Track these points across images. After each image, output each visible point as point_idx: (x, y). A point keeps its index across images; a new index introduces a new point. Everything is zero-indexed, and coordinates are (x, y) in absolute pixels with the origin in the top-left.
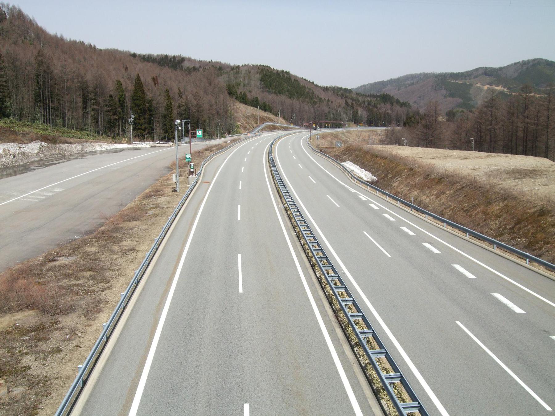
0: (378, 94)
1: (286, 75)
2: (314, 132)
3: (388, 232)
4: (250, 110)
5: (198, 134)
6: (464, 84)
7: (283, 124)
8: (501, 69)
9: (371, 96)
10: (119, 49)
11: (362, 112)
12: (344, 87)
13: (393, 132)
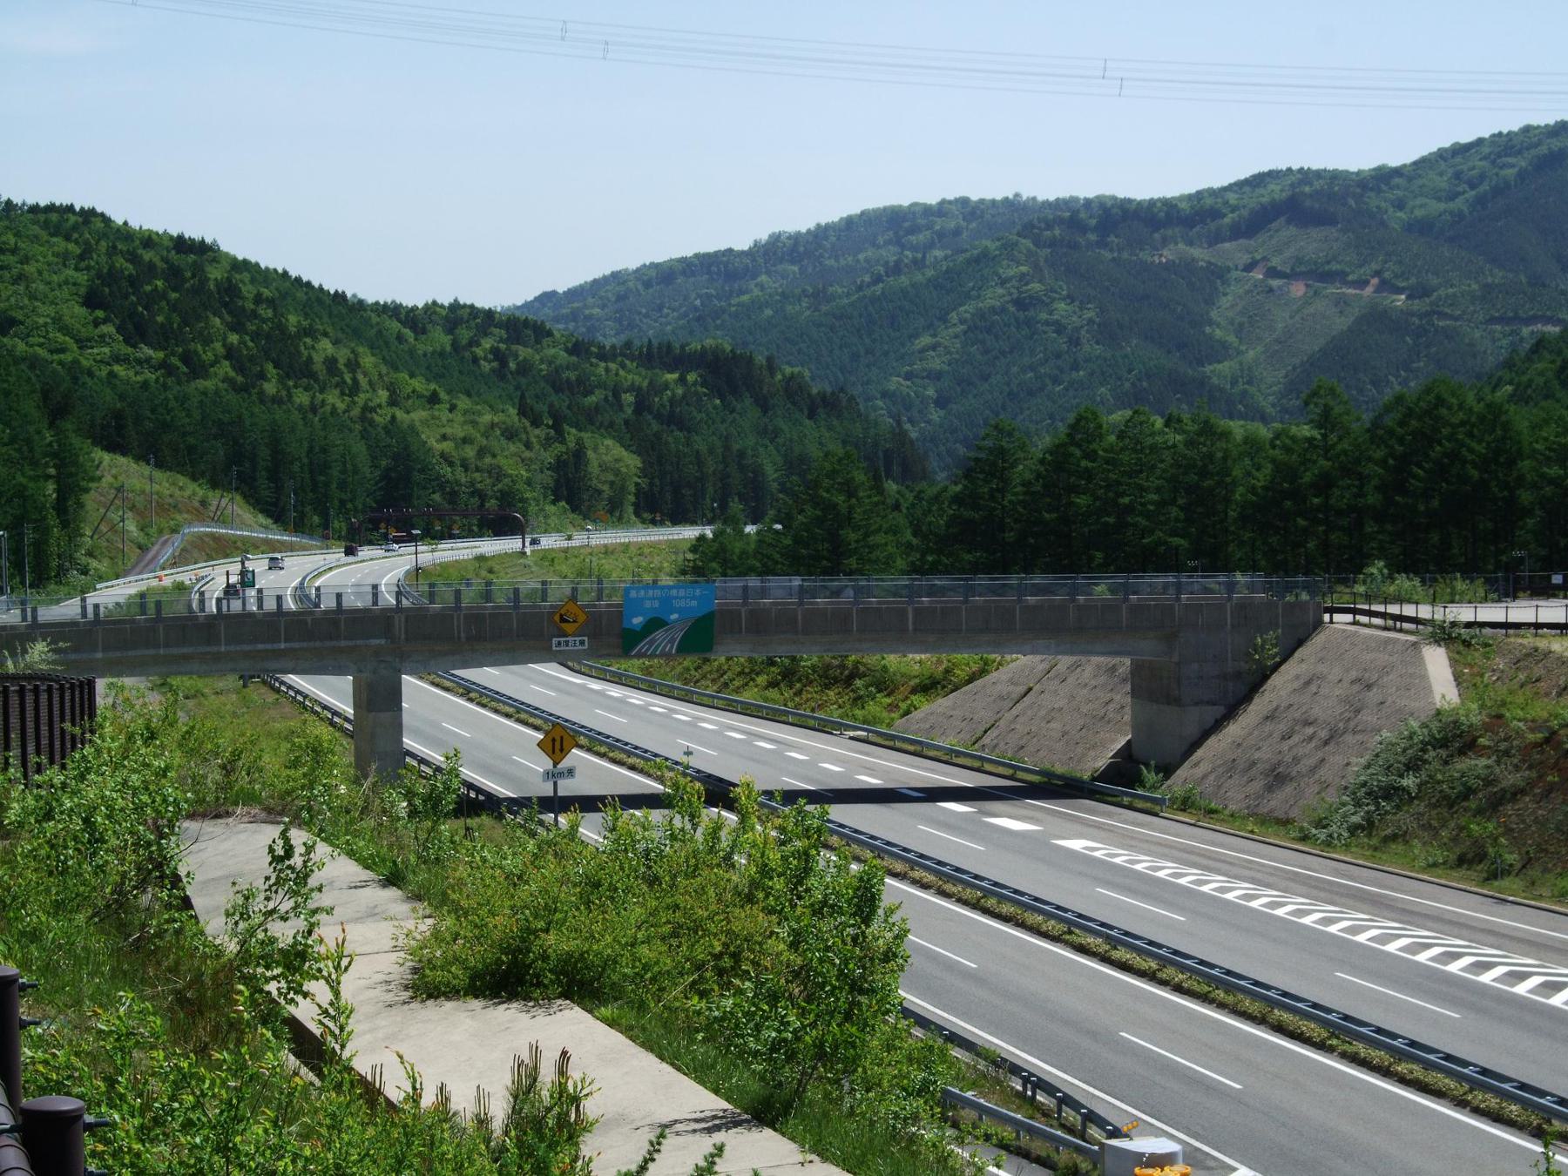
6: (1185, 268)
7: (250, 528)
8: (1383, 177)
11: (611, 457)
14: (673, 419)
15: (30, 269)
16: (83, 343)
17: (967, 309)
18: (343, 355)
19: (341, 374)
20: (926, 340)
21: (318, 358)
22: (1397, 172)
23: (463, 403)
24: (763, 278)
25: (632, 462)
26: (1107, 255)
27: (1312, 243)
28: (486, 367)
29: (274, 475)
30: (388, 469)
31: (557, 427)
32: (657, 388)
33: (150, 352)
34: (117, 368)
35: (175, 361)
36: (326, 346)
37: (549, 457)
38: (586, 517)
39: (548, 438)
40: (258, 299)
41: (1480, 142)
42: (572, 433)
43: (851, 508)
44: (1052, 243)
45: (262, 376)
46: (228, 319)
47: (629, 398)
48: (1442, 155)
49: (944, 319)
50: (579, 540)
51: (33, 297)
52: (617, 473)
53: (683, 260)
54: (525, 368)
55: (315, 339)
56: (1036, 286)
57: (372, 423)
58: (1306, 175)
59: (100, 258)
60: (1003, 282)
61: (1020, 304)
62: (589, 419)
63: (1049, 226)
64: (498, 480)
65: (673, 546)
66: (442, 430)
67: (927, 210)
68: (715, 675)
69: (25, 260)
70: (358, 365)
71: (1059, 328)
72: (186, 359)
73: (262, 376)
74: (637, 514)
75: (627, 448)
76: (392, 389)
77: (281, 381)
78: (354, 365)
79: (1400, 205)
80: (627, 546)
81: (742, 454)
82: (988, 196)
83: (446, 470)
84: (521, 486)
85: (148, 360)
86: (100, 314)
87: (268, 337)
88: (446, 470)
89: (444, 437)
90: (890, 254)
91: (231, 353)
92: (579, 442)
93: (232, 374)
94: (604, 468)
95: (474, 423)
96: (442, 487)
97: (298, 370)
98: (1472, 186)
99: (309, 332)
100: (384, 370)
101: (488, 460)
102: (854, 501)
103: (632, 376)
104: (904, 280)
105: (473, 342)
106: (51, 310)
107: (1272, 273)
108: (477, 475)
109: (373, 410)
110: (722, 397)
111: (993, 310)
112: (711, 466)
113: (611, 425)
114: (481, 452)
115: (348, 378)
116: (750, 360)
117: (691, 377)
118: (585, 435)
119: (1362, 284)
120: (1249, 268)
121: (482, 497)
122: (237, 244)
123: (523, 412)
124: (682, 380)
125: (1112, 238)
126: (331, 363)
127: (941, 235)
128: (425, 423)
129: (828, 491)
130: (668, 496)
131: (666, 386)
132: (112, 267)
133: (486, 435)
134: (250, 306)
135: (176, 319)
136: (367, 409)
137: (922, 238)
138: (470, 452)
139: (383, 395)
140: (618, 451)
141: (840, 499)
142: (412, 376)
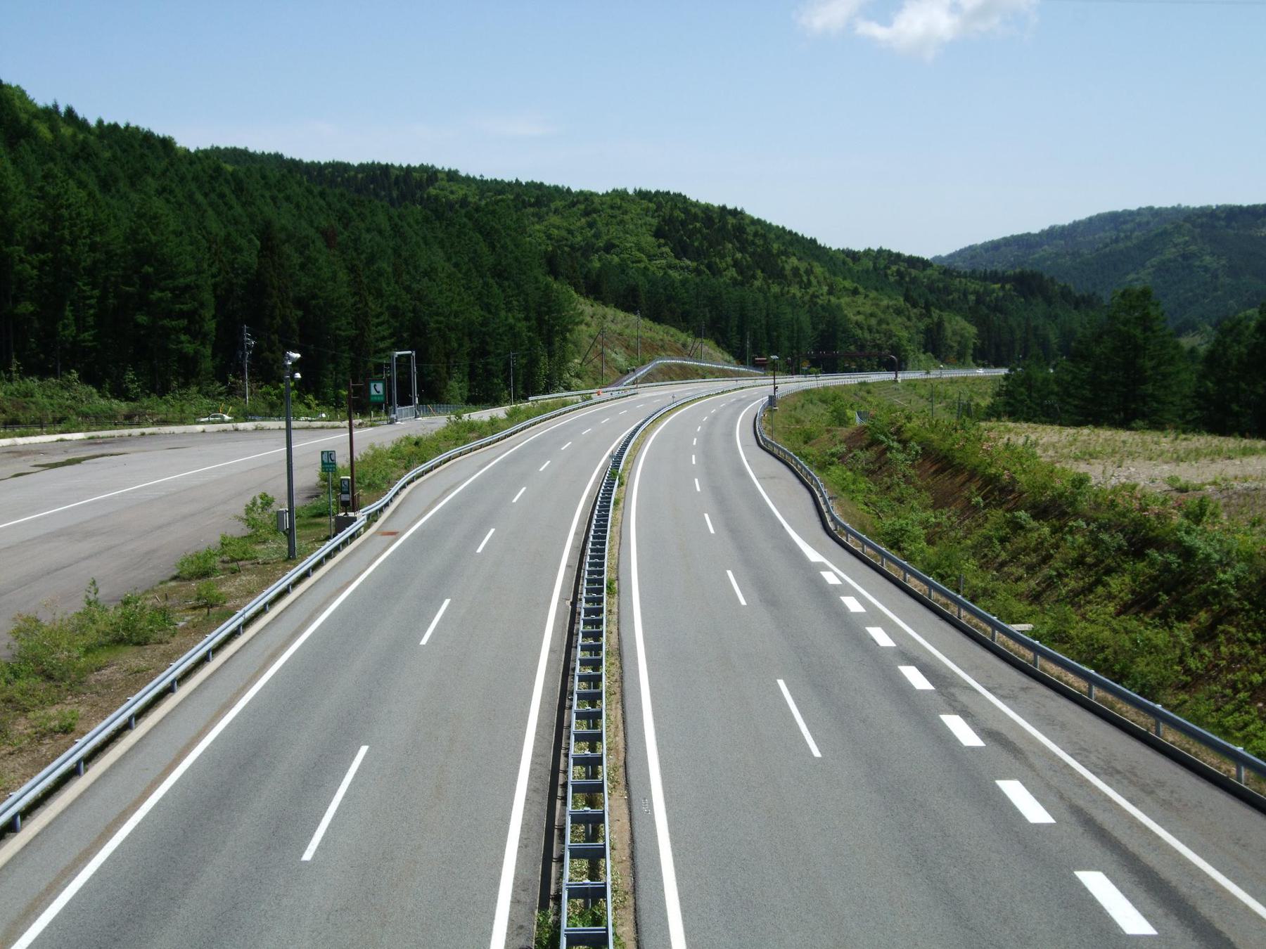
0: (1011, 272)
1: (67, 131)
2: (791, 384)
3: (839, 669)
5: (373, 392)
7: (713, 360)
9: (994, 277)
10: (251, 150)
11: (960, 327)
12: (907, 251)
13: (1027, 382)
14: (997, 308)
15: (627, 217)
16: (651, 258)
17: (1155, 260)
18: (803, 266)
19: (801, 276)
21: (788, 267)
23: (873, 294)
24: (1046, 247)
25: (972, 330)
26: (1231, 232)
28: (892, 279)
29: (741, 331)
30: (823, 331)
31: (927, 307)
32: (988, 293)
33: (689, 262)
34: (670, 272)
35: (702, 267)
36: (794, 261)
37: (922, 326)
38: (943, 362)
39: (921, 315)
40: (756, 234)
42: (936, 313)
43: (1147, 339)
44: (1202, 226)
46: (738, 245)
47: (972, 298)
49: (1143, 266)
50: (934, 374)
52: (962, 336)
53: (1005, 239)
54: (914, 280)
55: (788, 257)
56: (1193, 248)
57: (815, 304)
59: (666, 211)
60: (1175, 246)
61: (1185, 257)
62: (949, 306)
63: (1199, 217)
64: (890, 338)
66: (856, 310)
68: (1034, 558)
69: (625, 213)
70: (812, 272)
71: (1206, 269)
72: (709, 267)
73: (754, 277)
74: (974, 360)
75: (969, 322)
77: (764, 279)
78: (809, 272)
80: (966, 378)
81: (1036, 328)
82: (1164, 205)
84: (905, 343)
85: (687, 267)
86: (662, 241)
87: (760, 256)
89: (859, 313)
90: (1114, 234)
91: (736, 264)
92: (940, 317)
93: (735, 275)
94: (954, 333)
95: (877, 305)
96: (855, 342)
99: (785, 253)
100: (827, 275)
101: (884, 326)
103: (974, 286)
104: (1121, 245)
105: (887, 267)
108: (877, 336)
109: (817, 297)
110: (1025, 297)
111: (1170, 260)
112: (1018, 334)
113: (961, 309)
114: (880, 322)
115: (805, 279)
116: (1041, 276)
117: (1008, 286)
118: (945, 315)
121: (880, 348)
123: (907, 299)
124: (1003, 288)
125: (1234, 224)
126: (796, 271)
127: (1139, 225)
128: (848, 305)
130: (993, 351)
131: (994, 291)
132: (671, 215)
133: (884, 312)
134: (750, 238)
135: (706, 244)
137: (1129, 226)
138: (873, 321)
139: (825, 289)
141: (1138, 332)
142: (845, 279)
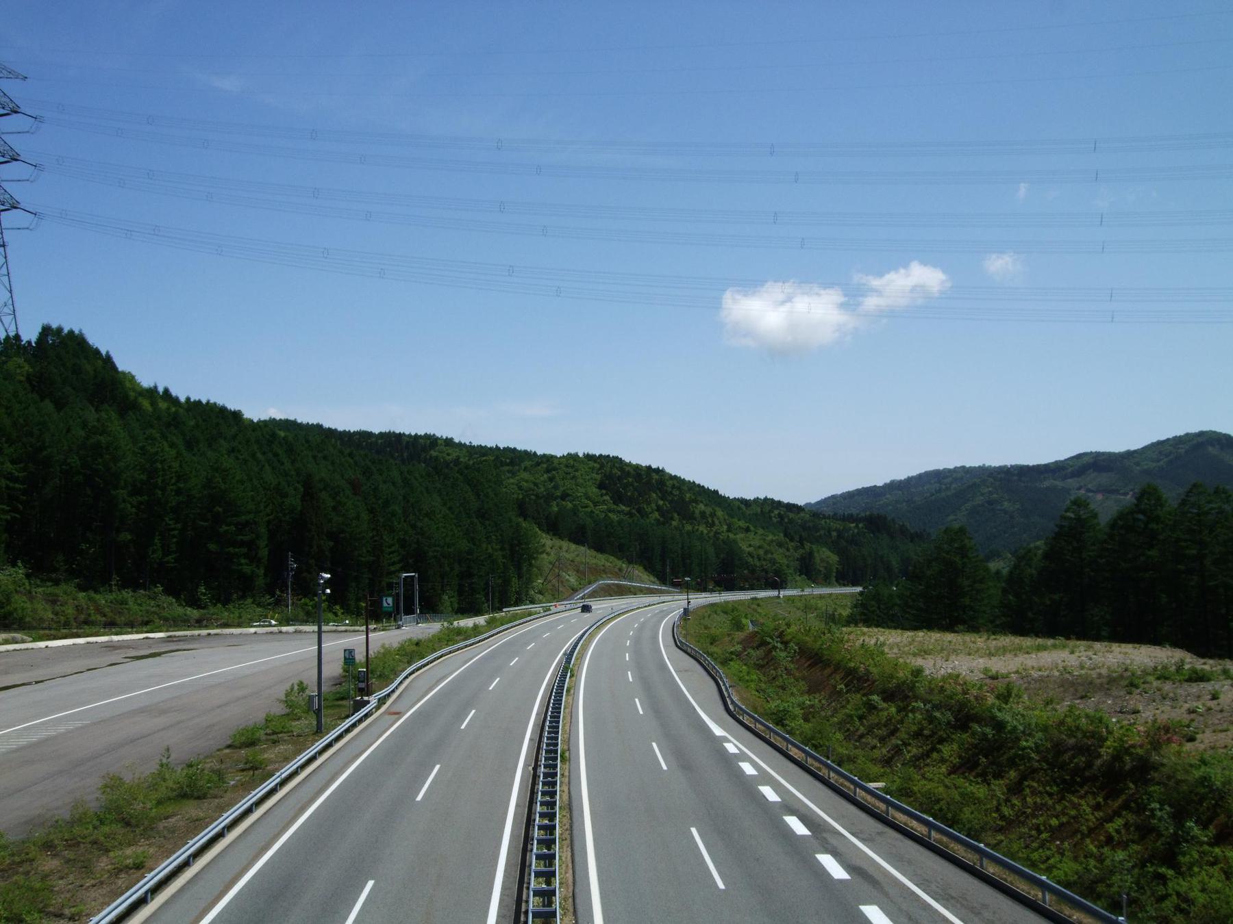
1: (163, 405)
2: (700, 599)
4: (571, 551)
5: (385, 604)
7: (642, 582)
8: (1129, 454)
9: (851, 518)
11: (826, 556)
12: (786, 498)
16: (595, 504)
17: (968, 505)
20: (952, 517)
21: (697, 512)
22: (1135, 451)
23: (761, 531)
27: (1104, 479)
31: (801, 541)
36: (702, 507)
37: (797, 555)
41: (1168, 440)
42: (807, 546)
45: (672, 519)
47: (834, 534)
48: (1153, 445)
50: (807, 591)
51: (577, 485)
54: (791, 521)
57: (718, 539)
58: (1098, 454)
65: (852, 595)
66: (748, 543)
67: (950, 471)
69: (577, 470)
71: (1005, 512)
72: (639, 511)
73: (672, 519)
76: (729, 526)
78: (713, 515)
79: (1138, 464)
83: (750, 559)
88: (750, 559)
91: (659, 509)
94: (822, 560)
97: (688, 517)
98: (1167, 456)
99: (696, 501)
102: (965, 560)
103: (837, 525)
104: (943, 494)
105: (770, 511)
106: (583, 490)
107: (1089, 490)
114: (766, 552)
117: (861, 525)
119: (1126, 494)
120: (1079, 489)
122: (672, 470)
123: (786, 535)
124: (857, 526)
126: (703, 514)
128: (742, 539)
129: (948, 553)
131: (850, 529)
133: (769, 545)
136: (716, 533)
138: (761, 552)
139: (725, 527)
140: (828, 553)
141: (957, 559)
